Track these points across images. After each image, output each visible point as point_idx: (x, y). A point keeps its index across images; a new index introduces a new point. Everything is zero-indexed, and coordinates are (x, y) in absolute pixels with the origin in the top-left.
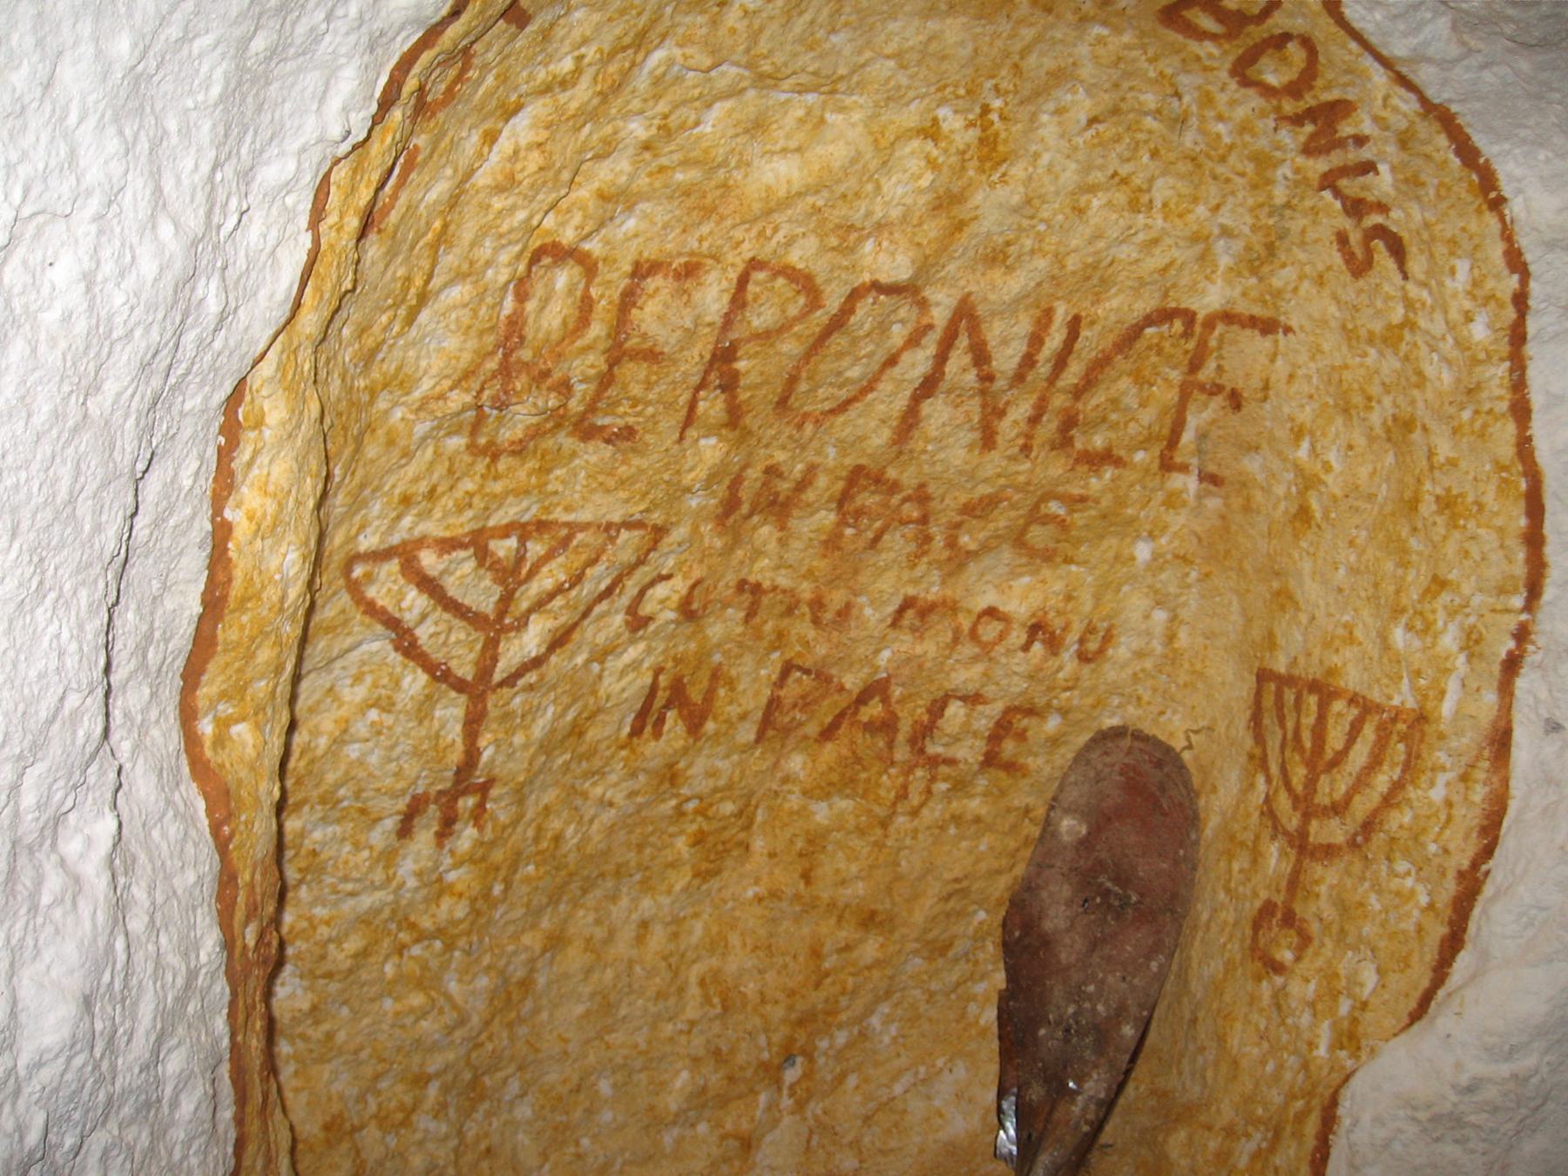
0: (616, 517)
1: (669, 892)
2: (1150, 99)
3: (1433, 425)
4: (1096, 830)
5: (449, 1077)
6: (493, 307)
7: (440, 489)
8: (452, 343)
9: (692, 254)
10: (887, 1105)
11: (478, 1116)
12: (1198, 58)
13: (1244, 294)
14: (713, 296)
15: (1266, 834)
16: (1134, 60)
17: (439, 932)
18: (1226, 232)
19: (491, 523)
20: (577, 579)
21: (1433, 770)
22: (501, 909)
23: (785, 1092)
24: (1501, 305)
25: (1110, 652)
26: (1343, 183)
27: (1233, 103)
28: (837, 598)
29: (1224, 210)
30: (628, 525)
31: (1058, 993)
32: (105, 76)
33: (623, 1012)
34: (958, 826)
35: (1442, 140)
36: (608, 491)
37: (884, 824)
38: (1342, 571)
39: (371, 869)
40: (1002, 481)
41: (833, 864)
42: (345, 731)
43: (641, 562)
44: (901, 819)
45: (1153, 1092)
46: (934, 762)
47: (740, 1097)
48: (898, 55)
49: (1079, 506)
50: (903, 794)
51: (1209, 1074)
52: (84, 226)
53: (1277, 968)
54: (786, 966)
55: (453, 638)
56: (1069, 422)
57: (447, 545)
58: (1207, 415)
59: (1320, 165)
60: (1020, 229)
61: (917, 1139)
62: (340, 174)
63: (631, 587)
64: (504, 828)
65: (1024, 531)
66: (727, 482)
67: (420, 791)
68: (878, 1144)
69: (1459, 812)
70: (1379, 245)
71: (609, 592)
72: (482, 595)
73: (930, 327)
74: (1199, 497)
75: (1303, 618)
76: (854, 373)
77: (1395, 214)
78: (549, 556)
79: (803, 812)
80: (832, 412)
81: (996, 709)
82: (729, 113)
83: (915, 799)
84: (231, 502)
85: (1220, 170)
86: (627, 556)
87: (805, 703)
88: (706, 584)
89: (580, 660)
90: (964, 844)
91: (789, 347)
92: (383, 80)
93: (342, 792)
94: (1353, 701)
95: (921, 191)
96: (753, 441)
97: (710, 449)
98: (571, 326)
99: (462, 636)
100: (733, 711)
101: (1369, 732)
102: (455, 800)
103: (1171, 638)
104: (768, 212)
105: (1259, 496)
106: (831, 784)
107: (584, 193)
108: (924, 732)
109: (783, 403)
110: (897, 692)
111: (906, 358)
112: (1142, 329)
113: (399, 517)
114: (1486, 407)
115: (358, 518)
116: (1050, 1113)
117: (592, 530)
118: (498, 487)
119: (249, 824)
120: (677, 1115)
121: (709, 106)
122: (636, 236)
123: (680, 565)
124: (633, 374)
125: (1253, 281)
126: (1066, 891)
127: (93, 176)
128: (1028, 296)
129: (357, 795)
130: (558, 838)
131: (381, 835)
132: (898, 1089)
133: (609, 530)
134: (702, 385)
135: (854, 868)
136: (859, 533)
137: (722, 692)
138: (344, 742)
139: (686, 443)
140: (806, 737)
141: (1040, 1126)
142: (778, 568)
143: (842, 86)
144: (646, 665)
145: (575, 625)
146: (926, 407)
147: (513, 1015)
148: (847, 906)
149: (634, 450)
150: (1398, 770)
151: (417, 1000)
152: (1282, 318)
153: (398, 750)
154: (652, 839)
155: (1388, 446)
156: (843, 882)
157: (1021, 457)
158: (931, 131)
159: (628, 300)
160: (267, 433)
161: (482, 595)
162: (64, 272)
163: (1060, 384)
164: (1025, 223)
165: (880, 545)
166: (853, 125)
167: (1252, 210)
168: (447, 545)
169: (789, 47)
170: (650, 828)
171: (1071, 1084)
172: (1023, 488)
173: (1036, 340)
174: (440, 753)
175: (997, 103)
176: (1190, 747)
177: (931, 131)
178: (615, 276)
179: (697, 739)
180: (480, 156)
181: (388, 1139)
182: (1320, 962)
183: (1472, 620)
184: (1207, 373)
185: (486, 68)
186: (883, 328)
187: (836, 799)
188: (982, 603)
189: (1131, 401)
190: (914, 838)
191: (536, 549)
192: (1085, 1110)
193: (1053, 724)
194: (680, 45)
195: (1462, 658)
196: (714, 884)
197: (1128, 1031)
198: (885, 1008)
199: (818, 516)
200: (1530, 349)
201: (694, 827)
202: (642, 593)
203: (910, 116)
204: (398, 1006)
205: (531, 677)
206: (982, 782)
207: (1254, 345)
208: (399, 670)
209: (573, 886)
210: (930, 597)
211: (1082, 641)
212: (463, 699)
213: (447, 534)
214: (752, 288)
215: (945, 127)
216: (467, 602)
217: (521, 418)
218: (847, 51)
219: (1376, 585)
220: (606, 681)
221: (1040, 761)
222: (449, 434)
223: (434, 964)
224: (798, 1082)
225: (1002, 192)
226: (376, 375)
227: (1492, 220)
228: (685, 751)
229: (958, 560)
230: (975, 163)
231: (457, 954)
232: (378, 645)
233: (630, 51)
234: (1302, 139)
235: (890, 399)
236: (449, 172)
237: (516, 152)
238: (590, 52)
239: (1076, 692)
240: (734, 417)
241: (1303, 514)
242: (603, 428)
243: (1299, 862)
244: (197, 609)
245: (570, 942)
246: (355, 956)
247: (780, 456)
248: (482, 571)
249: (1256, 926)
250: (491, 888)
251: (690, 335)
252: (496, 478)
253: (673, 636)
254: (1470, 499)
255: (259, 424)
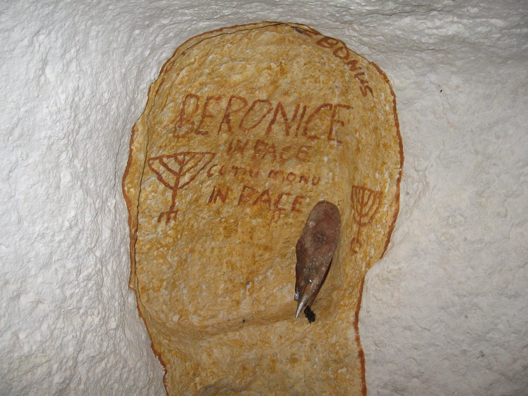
0: (205, 151)
1: (219, 241)
2: (317, 60)
3: (381, 129)
4: (317, 224)
5: (168, 280)
6: (178, 107)
7: (167, 145)
8: (170, 115)
9: (219, 95)
10: (272, 295)
11: (175, 291)
12: (326, 51)
13: (342, 100)
14: (224, 103)
15: (354, 222)
16: (313, 52)
17: (166, 245)
18: (337, 87)
19: (178, 152)
20: (196, 165)
21: (384, 204)
22: (180, 242)
23: (247, 291)
24: (391, 103)
25: (320, 183)
26: (359, 76)
27: (335, 60)
28: (255, 170)
29: (336, 82)
30: (207, 153)
31: (308, 261)
32: (121, 75)
33: (208, 269)
34: (287, 225)
35: (375, 69)
36: (203, 145)
37: (269, 225)
38: (367, 162)
39: (152, 229)
40: (291, 143)
41: (258, 234)
42: (147, 197)
43: (210, 161)
44: (273, 224)
45: (331, 285)
46: (280, 210)
47: (236, 291)
48: (260, 53)
49: (310, 148)
50: (273, 217)
51: (342, 279)
52: (117, 99)
53: (355, 252)
54: (247, 259)
55: (170, 177)
56: (306, 129)
57: (169, 157)
58: (337, 127)
59: (354, 73)
60: (291, 87)
61: (279, 303)
62: (153, 85)
63: (208, 167)
64: (180, 222)
65: (298, 154)
66: (229, 143)
67: (163, 211)
68: (270, 304)
69: (389, 213)
70: (367, 90)
71: (203, 168)
72: (176, 168)
73: (272, 109)
74: (337, 146)
75: (360, 173)
76: (256, 119)
77: (370, 83)
78: (190, 160)
79: (249, 222)
80: (252, 128)
81: (294, 197)
82: (226, 67)
83: (276, 219)
84: (133, 145)
85: (334, 74)
86: (207, 160)
87: (249, 196)
88: (225, 167)
89: (197, 183)
90: (288, 230)
91: (241, 114)
92: (161, 69)
93: (146, 211)
94: (369, 190)
95: (268, 80)
96: (234, 134)
97: (225, 136)
98: (194, 110)
99: (172, 177)
100: (232, 197)
101: (372, 197)
102: (170, 214)
103: (333, 179)
104: (235, 86)
105: (350, 146)
106: (256, 215)
107: (196, 84)
108: (277, 202)
109: (240, 126)
110: (270, 193)
111: (267, 116)
112: (320, 108)
113: (159, 151)
114: (390, 124)
115: (151, 151)
116: (306, 287)
117: (199, 154)
118: (179, 144)
119: (134, 208)
120: (221, 295)
121: (222, 65)
122: (207, 91)
123: (219, 162)
124: (207, 120)
125: (344, 97)
126: (310, 238)
127: (119, 91)
128: (294, 101)
129: (149, 212)
130: (192, 226)
131: (154, 221)
132: (275, 291)
133: (203, 154)
134: (222, 122)
135: (262, 236)
136: (259, 155)
137: (230, 193)
138: (147, 200)
139: (219, 135)
140: (250, 204)
141: (303, 291)
142: (241, 163)
143: (249, 60)
144: (212, 185)
145: (196, 175)
146: (273, 126)
147: (183, 268)
148: (261, 245)
149: (208, 136)
150: (377, 205)
151: (161, 261)
152: (351, 105)
153: (158, 202)
154: (214, 228)
155: (374, 133)
156: (260, 239)
157: (295, 137)
158: (269, 68)
159: (206, 105)
160: (139, 132)
161: (176, 168)
162: (114, 106)
163: (303, 121)
164: (292, 86)
165: (265, 158)
166: (253, 67)
167: (342, 82)
168: (169, 157)
169: (237, 54)
170: (214, 225)
171: (310, 281)
172: (296, 144)
173: (296, 111)
174: (167, 202)
175: (283, 62)
176: (339, 205)
177: (269, 68)
178: (203, 100)
179: (224, 204)
180: (176, 78)
181: (155, 294)
182: (363, 250)
183: (391, 171)
184: (336, 118)
185: (177, 63)
186: (262, 109)
187: (257, 219)
188: (289, 171)
189: (319, 124)
190: (276, 228)
191: (187, 158)
192: (313, 286)
193: (308, 200)
194: (215, 54)
195: (389, 179)
196: (229, 239)
197: (324, 269)
198: (271, 271)
199: (250, 151)
200: (398, 112)
201: (224, 225)
202: (211, 169)
203: (265, 65)
204: (157, 262)
205: (187, 187)
206: (292, 215)
207: (346, 111)
208: (158, 184)
209: (196, 238)
210: (277, 170)
211: (313, 180)
212: (172, 191)
213: (169, 154)
214: (232, 102)
215: (272, 67)
216: (173, 169)
217: (184, 129)
218: (250, 53)
219: (373, 164)
220: (203, 189)
221: (305, 209)
222: (169, 133)
223: (165, 253)
224: (250, 288)
225: (286, 80)
226: (155, 121)
227: (387, 85)
228: (222, 206)
229: (283, 161)
230: (279, 74)
231: (170, 251)
232: (154, 178)
233: (205, 57)
234: (350, 67)
235: (265, 125)
236: (170, 82)
237: (183, 77)
238: (197, 57)
239: (312, 192)
240: (230, 129)
241: (358, 149)
242: (201, 132)
243: (359, 227)
244: (126, 165)
245: (195, 251)
246: (148, 249)
247: (241, 138)
248: (176, 163)
249: (352, 243)
250: (178, 236)
251: (219, 112)
252: (179, 142)
253: (218, 179)
254: (389, 144)
255: (138, 131)
